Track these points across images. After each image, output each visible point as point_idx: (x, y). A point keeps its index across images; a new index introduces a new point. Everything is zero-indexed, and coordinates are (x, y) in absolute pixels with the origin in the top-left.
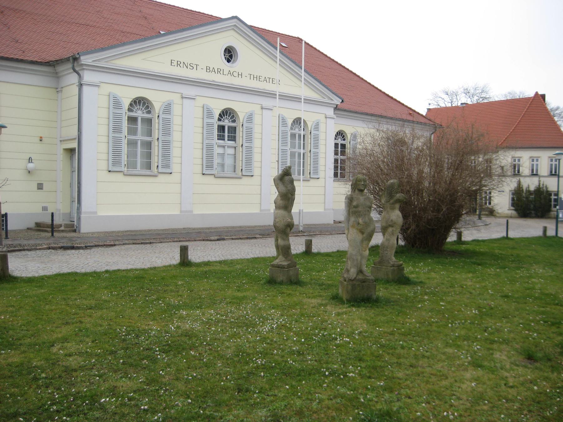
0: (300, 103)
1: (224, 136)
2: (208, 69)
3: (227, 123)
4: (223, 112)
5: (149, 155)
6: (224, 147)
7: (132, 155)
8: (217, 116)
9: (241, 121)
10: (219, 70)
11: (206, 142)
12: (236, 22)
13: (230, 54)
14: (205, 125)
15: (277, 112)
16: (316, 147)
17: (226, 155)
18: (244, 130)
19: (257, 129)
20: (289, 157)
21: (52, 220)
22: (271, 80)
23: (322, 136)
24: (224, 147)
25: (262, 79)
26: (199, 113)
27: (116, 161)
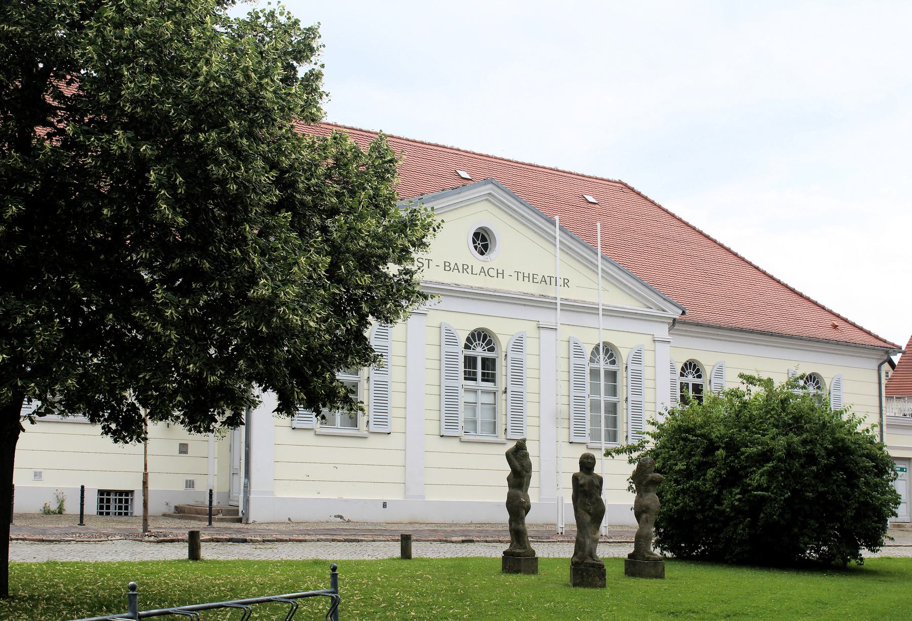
0: (554, 311)
1: (475, 374)
2: (447, 266)
3: (479, 352)
4: (473, 334)
5: (613, 422)
6: (475, 391)
7: (595, 421)
8: (463, 341)
9: (504, 350)
10: (465, 267)
11: (444, 383)
12: (492, 189)
13: (482, 240)
14: (443, 357)
15: (566, 333)
16: (638, 391)
17: (479, 405)
18: (509, 364)
19: (530, 362)
20: (588, 409)
22: (553, 280)
23: (647, 373)
24: (475, 391)
25: (539, 279)
26: (433, 336)
27: (451, 423)
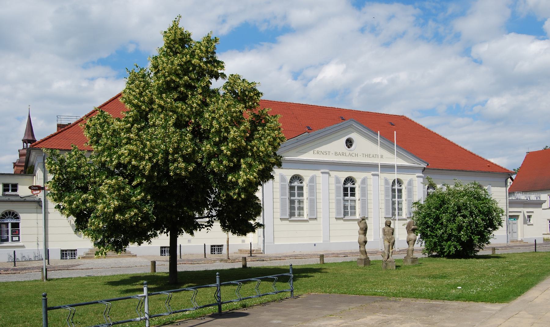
2: (336, 154)
4: (346, 179)
13: (349, 143)
21: (53, 308)
25: (371, 156)
